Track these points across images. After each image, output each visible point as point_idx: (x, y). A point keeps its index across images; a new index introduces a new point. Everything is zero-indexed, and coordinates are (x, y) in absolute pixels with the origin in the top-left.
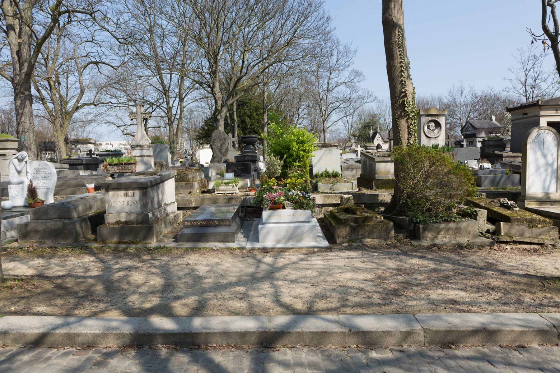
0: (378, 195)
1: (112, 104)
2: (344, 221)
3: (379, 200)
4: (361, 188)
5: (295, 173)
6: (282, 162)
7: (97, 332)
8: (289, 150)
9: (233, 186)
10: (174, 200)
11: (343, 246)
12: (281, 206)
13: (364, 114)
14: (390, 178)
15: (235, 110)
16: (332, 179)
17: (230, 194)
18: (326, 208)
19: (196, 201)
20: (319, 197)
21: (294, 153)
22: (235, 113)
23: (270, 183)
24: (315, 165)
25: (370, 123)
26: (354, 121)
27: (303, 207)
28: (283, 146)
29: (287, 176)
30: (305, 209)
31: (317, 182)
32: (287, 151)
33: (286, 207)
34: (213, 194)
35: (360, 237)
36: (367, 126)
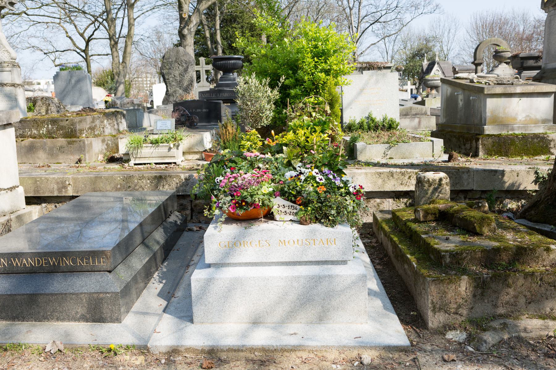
0: (503, 173)
1: (28, 15)
2: (448, 260)
3: (507, 184)
4: (455, 154)
5: (306, 118)
6: (276, 92)
7: (147, 259)
8: (295, 72)
9: (170, 149)
10: (16, 182)
11: (449, 341)
12: (262, 212)
13: (410, 39)
14: (517, 132)
15: (218, 27)
16: (385, 135)
17: (163, 166)
18: (378, 200)
19: (75, 183)
20: (363, 176)
21: (306, 78)
22: (218, 32)
23: (243, 142)
24: (350, 104)
25: (422, 50)
26: (395, 50)
27: (326, 216)
28: (281, 61)
29: (285, 124)
30: (333, 223)
31: (354, 140)
32: (290, 72)
33: (277, 217)
34: (126, 165)
35: (501, 311)
36: (418, 54)
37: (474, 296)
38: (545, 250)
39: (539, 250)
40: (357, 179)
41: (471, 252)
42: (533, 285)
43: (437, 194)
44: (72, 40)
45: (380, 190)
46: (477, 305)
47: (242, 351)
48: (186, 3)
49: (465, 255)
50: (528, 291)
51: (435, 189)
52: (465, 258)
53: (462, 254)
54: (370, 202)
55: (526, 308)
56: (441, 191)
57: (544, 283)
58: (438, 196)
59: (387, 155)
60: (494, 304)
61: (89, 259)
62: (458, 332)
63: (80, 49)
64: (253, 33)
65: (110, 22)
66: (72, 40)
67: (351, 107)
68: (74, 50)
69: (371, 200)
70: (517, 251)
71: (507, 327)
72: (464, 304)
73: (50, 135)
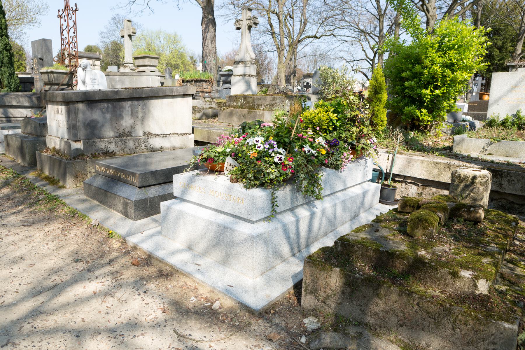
20: (419, 163)
24: (497, 101)
37: (343, 293)
38: (450, 273)
39: (443, 271)
40: (413, 165)
41: (363, 248)
42: (408, 307)
43: (468, 192)
44: (365, 52)
45: (434, 179)
46: (345, 303)
47: (162, 263)
48: (433, 19)
49: (356, 248)
50: (402, 311)
51: (467, 187)
52: (356, 252)
53: (353, 246)
54: (425, 189)
55: (397, 329)
56: (472, 190)
57: (421, 309)
58: (469, 194)
59: (486, 150)
60: (362, 310)
61: (130, 177)
62: (315, 321)
63: (370, 59)
64: (514, 43)
65: (381, 38)
66: (365, 52)
67: (498, 103)
68: (366, 60)
69: (426, 187)
70: (413, 263)
71: (360, 339)
72: (332, 296)
73: (242, 107)
